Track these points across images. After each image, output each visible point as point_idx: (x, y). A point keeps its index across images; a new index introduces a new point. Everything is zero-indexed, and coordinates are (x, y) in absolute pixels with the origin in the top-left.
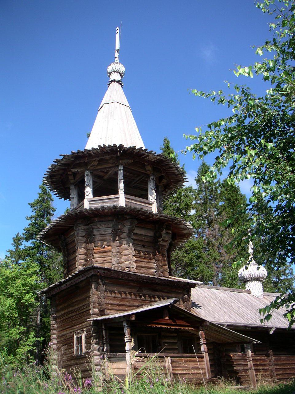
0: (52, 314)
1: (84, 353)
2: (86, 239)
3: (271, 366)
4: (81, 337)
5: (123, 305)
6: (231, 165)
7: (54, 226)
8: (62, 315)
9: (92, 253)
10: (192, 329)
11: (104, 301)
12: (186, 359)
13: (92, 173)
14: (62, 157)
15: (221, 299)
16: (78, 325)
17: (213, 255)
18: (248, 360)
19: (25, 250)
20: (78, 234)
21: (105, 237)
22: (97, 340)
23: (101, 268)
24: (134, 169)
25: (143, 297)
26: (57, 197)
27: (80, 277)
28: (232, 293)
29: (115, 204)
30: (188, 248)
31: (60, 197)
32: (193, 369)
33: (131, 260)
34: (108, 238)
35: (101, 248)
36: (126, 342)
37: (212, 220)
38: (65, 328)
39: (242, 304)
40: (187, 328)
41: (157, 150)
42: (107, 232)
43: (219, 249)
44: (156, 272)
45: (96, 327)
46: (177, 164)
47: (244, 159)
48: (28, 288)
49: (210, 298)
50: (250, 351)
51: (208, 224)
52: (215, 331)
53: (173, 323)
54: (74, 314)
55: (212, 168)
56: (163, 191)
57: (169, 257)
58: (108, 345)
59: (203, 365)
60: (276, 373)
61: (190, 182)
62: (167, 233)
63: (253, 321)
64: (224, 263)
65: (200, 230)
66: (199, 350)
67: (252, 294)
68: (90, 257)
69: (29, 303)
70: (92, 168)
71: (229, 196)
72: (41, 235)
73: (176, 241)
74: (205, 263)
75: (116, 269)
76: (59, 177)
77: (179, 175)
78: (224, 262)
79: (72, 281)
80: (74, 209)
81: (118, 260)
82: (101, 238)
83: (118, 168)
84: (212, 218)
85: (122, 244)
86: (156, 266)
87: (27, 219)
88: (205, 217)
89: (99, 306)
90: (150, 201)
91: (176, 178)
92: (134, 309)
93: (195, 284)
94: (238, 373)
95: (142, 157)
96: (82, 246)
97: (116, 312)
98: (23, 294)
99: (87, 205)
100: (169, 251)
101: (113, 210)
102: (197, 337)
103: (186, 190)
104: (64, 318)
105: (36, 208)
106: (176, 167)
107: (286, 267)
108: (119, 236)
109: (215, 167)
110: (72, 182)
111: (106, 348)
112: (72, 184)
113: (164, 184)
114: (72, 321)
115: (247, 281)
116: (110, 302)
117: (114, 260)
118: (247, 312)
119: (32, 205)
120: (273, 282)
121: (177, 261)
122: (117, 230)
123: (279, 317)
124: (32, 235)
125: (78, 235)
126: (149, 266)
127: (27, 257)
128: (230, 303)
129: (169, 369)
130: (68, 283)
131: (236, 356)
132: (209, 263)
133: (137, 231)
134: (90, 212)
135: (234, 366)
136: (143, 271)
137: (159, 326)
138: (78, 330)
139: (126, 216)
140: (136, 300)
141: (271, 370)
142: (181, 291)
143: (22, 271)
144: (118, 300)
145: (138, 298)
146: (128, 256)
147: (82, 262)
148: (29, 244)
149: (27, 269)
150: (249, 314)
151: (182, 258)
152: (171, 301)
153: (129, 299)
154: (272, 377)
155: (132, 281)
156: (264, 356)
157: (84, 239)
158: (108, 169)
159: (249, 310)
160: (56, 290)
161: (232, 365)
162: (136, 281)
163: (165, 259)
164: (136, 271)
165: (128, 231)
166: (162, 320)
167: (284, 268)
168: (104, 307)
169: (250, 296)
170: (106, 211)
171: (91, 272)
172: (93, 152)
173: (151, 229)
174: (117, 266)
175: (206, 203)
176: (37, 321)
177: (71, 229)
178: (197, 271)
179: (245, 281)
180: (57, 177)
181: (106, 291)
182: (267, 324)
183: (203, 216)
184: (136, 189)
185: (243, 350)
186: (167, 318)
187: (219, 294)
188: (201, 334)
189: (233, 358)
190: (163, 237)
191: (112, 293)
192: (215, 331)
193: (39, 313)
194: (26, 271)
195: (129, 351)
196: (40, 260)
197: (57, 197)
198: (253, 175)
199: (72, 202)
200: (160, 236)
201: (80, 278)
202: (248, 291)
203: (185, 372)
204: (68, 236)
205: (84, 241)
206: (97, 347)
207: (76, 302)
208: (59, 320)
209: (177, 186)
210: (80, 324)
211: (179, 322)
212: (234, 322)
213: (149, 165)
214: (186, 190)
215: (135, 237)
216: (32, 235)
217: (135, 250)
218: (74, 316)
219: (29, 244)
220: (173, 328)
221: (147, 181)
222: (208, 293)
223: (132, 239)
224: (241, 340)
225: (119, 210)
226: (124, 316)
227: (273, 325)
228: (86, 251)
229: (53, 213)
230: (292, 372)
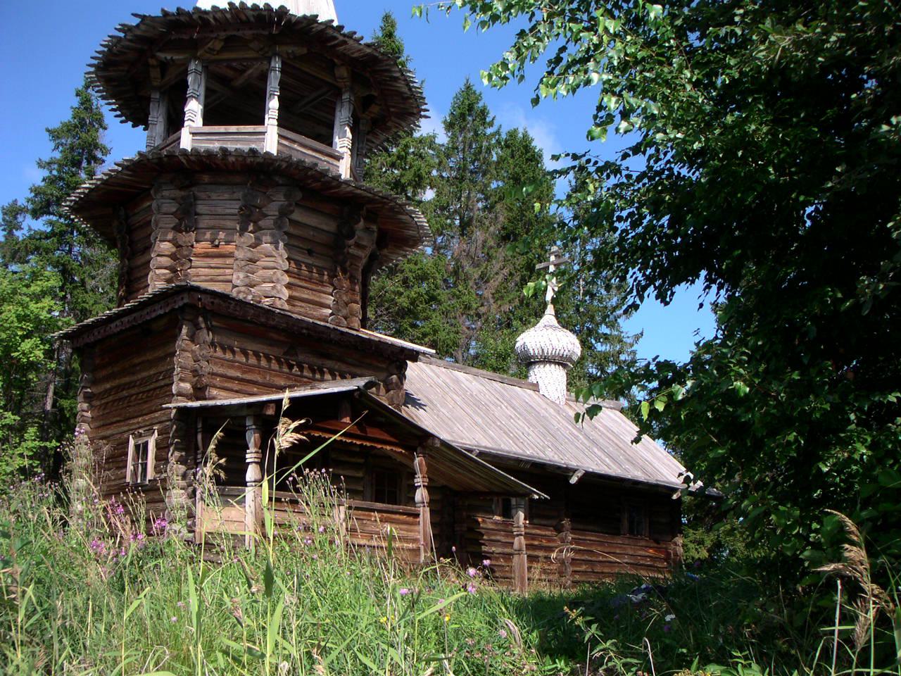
0: (83, 387)
1: (149, 481)
2: (177, 221)
4: (146, 445)
5: (249, 382)
6: (553, 56)
7: (104, 182)
8: (106, 391)
9: (188, 256)
10: (400, 450)
11: (206, 367)
13: (205, 68)
14: (138, 20)
15: (472, 395)
16: (140, 416)
17: (464, 298)
18: (515, 533)
19: (31, 238)
20: (159, 207)
21: (222, 222)
22: (183, 453)
23: (205, 292)
24: (308, 70)
25: (295, 369)
26: (116, 116)
27: (156, 308)
28: (497, 385)
29: (253, 146)
31: (124, 118)
34: (229, 224)
35: (210, 246)
36: (249, 463)
37: (471, 219)
38: (109, 422)
40: (388, 448)
41: (367, 32)
42: (228, 211)
43: (479, 288)
44: (331, 314)
46: (410, 72)
47: (589, 38)
48: (30, 326)
49: (447, 390)
50: (522, 515)
51: (460, 226)
53: (359, 433)
54: (133, 391)
55: (508, 54)
56: (368, 133)
57: (365, 285)
61: (432, 127)
62: (367, 229)
63: (536, 449)
64: (486, 320)
65: (439, 239)
66: (411, 500)
67: (541, 392)
68: (182, 265)
69: (31, 359)
70: (208, 55)
71: (517, 169)
72: (71, 201)
73: (385, 251)
75: (241, 296)
76: (126, 68)
77: (411, 98)
78: (485, 317)
79: (134, 315)
80: (155, 148)
81: (248, 276)
82: (212, 223)
83: (270, 63)
84: (472, 214)
85: (262, 241)
87: (41, 165)
88: (456, 211)
89: (194, 376)
90: (338, 152)
91: (402, 106)
92: (273, 393)
93: (418, 353)
95: (329, 44)
97: (230, 394)
98: (18, 338)
99: (186, 141)
100: (367, 272)
101: (249, 160)
102: (408, 470)
103: (421, 142)
104: (111, 398)
105: (63, 141)
106: (406, 80)
107: (622, 348)
108: (255, 223)
109: (515, 53)
110: (155, 84)
112: (155, 89)
113: (372, 115)
114: (129, 406)
115: (535, 363)
116: (221, 370)
117: (238, 277)
118: (527, 429)
119: (54, 134)
120: (590, 376)
121: (382, 300)
122: (253, 208)
123: (596, 450)
124: (48, 204)
125: (159, 210)
126: (318, 299)
127: (33, 254)
128: (491, 405)
130: (125, 319)
131: (490, 521)
133: (297, 216)
134: (193, 158)
135: (484, 544)
138: (140, 428)
139: (277, 179)
140: (280, 374)
142: (384, 366)
143: (17, 285)
144: (239, 368)
145: (286, 370)
146: (271, 272)
147: (164, 274)
148: (41, 225)
149: (32, 282)
150: (529, 434)
152: (360, 382)
153: (264, 368)
154: (561, 574)
155: (274, 328)
156: (552, 528)
158: (245, 64)
160: (96, 333)
161: (478, 540)
163: (357, 288)
164: (286, 307)
165: (277, 213)
166: (333, 422)
168: (205, 380)
169: (536, 397)
170: (232, 159)
171: (182, 299)
172: (215, 18)
174: (244, 292)
175: (462, 179)
176: (45, 404)
177: (145, 194)
178: (423, 330)
179: (528, 362)
180: (121, 68)
181: (212, 344)
183: (452, 208)
184: (306, 118)
185: (507, 513)
187: (467, 383)
190: (356, 237)
193: (52, 387)
194: (28, 286)
195: (254, 484)
196: (63, 265)
197: (116, 116)
198: (605, 77)
199: (151, 131)
200: (351, 235)
201: (154, 311)
202: (533, 384)
204: (136, 211)
205: (172, 226)
206: (182, 468)
207: (139, 364)
208: (98, 403)
209: (403, 124)
210: (146, 414)
211: (373, 432)
212: (495, 446)
213: (342, 65)
214: (421, 141)
215: (292, 230)
216: (48, 204)
217: (288, 259)
218: (132, 395)
219: (41, 225)
220: (358, 443)
221: (335, 104)
222: (443, 376)
223: (286, 233)
224: (504, 486)
225: (262, 160)
226: (250, 405)
227: (579, 464)
228: (174, 250)
229: (104, 158)
230: (606, 570)
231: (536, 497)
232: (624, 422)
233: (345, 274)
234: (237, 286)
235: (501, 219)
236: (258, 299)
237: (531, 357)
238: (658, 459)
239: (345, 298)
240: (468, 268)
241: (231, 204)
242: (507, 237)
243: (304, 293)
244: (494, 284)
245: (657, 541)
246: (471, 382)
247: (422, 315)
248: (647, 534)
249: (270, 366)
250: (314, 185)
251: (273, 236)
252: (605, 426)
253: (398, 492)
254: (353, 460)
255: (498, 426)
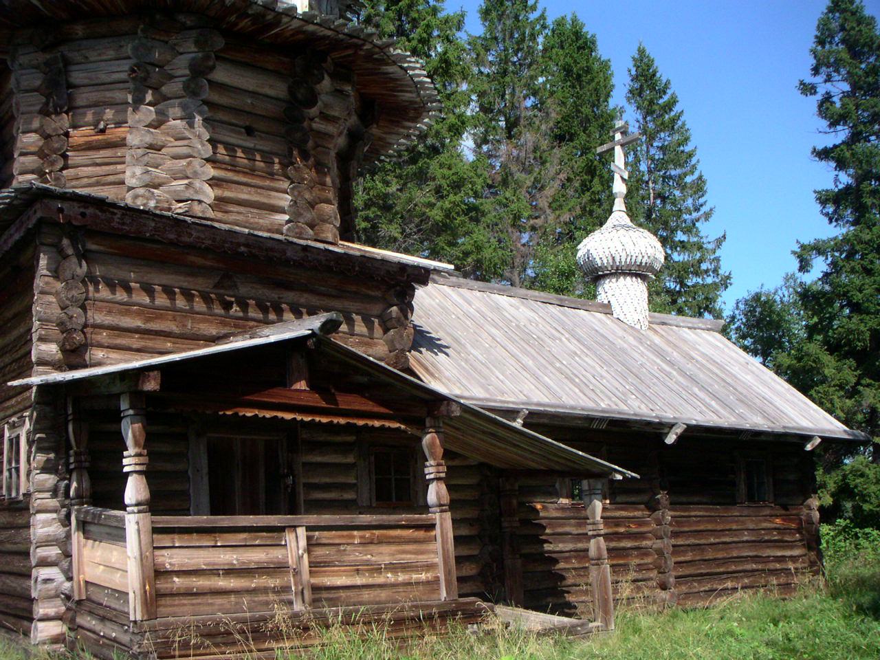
1: (24, 495)
2: (44, 100)
3: (661, 538)
4: (18, 437)
10: (397, 425)
12: (367, 534)
21: (108, 94)
22: (52, 456)
25: (235, 308)
28: (554, 310)
30: (444, 183)
32: (392, 567)
33: (196, 175)
34: (118, 95)
36: (128, 474)
39: (584, 345)
44: (288, 222)
45: (48, 409)
52: (484, 432)
53: (323, 404)
58: (86, 478)
59: (426, 555)
60: (674, 560)
62: (339, 93)
63: (614, 399)
67: (615, 315)
68: (52, 163)
71: (568, 60)
73: (375, 130)
74: (488, 226)
81: (148, 172)
85: (168, 117)
86: (292, 200)
89: (63, 333)
94: (556, 561)
96: (31, 123)
97: (127, 355)
108: (156, 89)
111: (74, 485)
115: (604, 276)
118: (599, 369)
122: (149, 68)
123: (696, 390)
125: (19, 87)
128: (546, 339)
129: (297, 573)
131: (552, 508)
132: (500, 226)
133: (222, 74)
136: (240, 218)
137: (268, 414)
139: (182, 18)
141: (660, 553)
142: (378, 294)
144: (138, 314)
145: (219, 310)
146: (184, 162)
151: (424, 209)
153: (181, 310)
155: (192, 248)
156: (643, 506)
157: (37, 100)
159: (605, 362)
162: (207, 249)
163: (328, 180)
164: (210, 214)
165: (187, 72)
167: (697, 257)
169: (609, 322)
171: (35, 212)
173: (276, 73)
175: (504, 73)
178: (463, 248)
179: (595, 275)
182: (658, 413)
186: (302, 385)
187: (512, 310)
188: (432, 445)
189: (541, 514)
190: (320, 103)
191: (118, 288)
192: (484, 432)
195: (136, 509)
200: (312, 100)
203: (359, 581)
205: (38, 108)
211: (348, 401)
215: (215, 97)
222: (477, 304)
223: (205, 102)
231: (619, 477)
232: (729, 348)
233: (307, 161)
234: (133, 188)
235: (553, 115)
236: (166, 205)
237: (597, 269)
238: (778, 394)
239: (307, 196)
240: (519, 176)
241: (119, 65)
242: (561, 138)
243: (242, 192)
244: (549, 191)
245: (785, 507)
246: (518, 309)
247: (461, 230)
248: (772, 499)
249: (192, 308)
250: (242, 24)
251: (184, 107)
252: (704, 355)
253: (412, 480)
254: (339, 439)
255: (559, 370)
